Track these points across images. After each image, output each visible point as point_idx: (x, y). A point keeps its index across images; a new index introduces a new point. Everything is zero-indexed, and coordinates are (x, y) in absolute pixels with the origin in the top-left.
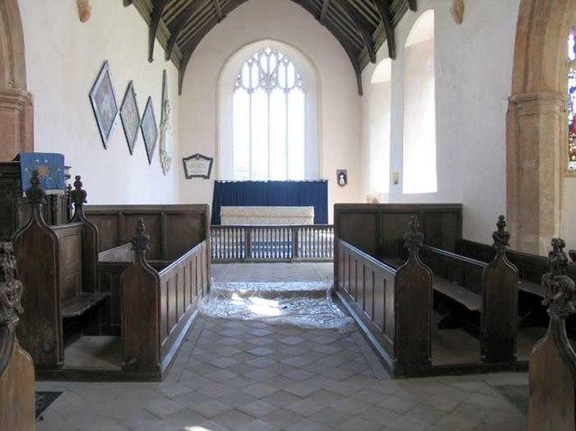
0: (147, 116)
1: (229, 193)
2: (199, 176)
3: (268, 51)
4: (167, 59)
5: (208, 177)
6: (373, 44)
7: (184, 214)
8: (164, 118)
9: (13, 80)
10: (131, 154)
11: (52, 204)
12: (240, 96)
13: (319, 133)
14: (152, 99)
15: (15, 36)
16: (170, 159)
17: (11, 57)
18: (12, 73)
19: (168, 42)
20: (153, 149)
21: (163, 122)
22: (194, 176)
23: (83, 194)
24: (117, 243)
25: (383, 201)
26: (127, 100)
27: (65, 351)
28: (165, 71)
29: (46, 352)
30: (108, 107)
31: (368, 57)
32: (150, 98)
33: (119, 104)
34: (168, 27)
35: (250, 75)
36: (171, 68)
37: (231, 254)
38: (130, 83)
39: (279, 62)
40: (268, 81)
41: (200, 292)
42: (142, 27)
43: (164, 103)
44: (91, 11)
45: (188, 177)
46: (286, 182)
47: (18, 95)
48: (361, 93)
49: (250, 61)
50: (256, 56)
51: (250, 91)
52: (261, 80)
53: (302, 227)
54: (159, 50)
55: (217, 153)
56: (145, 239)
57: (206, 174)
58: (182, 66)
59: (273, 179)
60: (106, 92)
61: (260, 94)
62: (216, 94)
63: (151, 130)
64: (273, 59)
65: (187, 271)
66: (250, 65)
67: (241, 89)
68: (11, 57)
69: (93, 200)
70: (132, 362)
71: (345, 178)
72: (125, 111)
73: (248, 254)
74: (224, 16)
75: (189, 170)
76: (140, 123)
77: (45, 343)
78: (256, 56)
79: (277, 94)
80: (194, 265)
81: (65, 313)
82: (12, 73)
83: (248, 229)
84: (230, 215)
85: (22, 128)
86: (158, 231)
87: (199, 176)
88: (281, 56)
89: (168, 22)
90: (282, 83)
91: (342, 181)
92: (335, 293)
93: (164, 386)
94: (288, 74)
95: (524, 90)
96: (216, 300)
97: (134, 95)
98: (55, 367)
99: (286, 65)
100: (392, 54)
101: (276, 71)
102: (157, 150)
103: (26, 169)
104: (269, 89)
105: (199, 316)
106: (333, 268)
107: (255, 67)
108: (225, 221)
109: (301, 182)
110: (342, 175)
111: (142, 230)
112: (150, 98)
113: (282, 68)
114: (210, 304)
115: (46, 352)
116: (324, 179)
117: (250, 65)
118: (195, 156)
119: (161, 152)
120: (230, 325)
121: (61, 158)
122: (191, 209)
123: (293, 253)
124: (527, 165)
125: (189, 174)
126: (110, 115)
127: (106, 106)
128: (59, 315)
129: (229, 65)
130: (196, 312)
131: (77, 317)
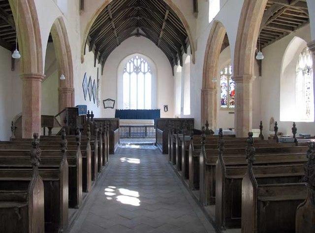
1: (123, 114)
2: (109, 107)
3: (137, 57)
5: (113, 108)
6: (186, 44)
12: (126, 75)
13: (157, 87)
21: (98, 87)
23: (93, 115)
25: (180, 117)
30: (91, 89)
31: (183, 51)
35: (130, 67)
36: (99, 66)
39: (141, 62)
40: (137, 69)
43: (98, 80)
46: (144, 110)
48: (173, 75)
49: (130, 61)
50: (132, 59)
51: (130, 73)
52: (134, 69)
53: (148, 126)
55: (116, 98)
58: (103, 64)
59: (139, 109)
61: (134, 75)
62: (117, 77)
64: (139, 61)
66: (130, 63)
67: (126, 73)
69: (95, 117)
71: (167, 108)
73: (130, 135)
74: (120, 44)
78: (132, 59)
79: (141, 74)
83: (130, 127)
84: (123, 122)
85: (72, 97)
87: (109, 107)
88: (142, 59)
90: (143, 70)
91: (166, 109)
92: (155, 145)
94: (145, 67)
95: (205, 88)
99: (144, 63)
100: (181, 65)
101: (140, 65)
104: (137, 73)
106: (124, 108)
107: (132, 64)
108: (120, 125)
109: (150, 110)
110: (166, 107)
113: (143, 64)
116: (159, 108)
117: (130, 63)
118: (108, 100)
121: (86, 106)
123: (145, 135)
124: (206, 108)
125: (106, 106)
129: (121, 64)
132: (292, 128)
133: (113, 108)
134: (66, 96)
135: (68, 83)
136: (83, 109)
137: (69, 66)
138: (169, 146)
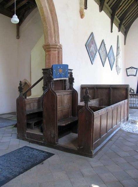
0: (110, 52)
4: (119, 31)
7: (118, 88)
8: (118, 53)
9: (55, 41)
10: (103, 67)
11: (65, 83)
14: (112, 46)
15: (56, 25)
16: (120, 69)
17: (55, 33)
18: (55, 38)
19: (112, 15)
20: (113, 65)
21: (117, 55)
22: (130, 75)
24: (93, 98)
26: (102, 47)
27: (59, 140)
28: (118, 36)
29: (52, 138)
32: (111, 46)
33: (98, 48)
34: (119, 19)
36: (121, 35)
37: (134, 105)
38: (92, 33)
41: (122, 120)
42: (109, 20)
44: (85, 14)
45: (128, 76)
47: (56, 46)
54: (115, 28)
56: (88, 97)
57: (135, 74)
58: (125, 34)
60: (92, 44)
63: (112, 58)
65: (116, 111)
68: (55, 33)
70: (81, 147)
72: (100, 51)
75: (128, 73)
76: (107, 55)
77: (52, 135)
80: (119, 110)
81: (59, 124)
82: (55, 38)
85: (59, 57)
86: (109, 94)
89: (111, 6)
93: (93, 161)
96: (130, 124)
97: (104, 45)
98: (55, 144)
102: (115, 65)
103: (55, 70)
105: (120, 130)
111: (87, 93)
112: (111, 46)
114: (127, 125)
115: (52, 138)
118: (130, 68)
119: (116, 66)
120: (133, 136)
122: (122, 86)
125: (128, 74)
126: (94, 52)
127: (92, 49)
128: (56, 125)
130: (119, 128)
131: (63, 126)
132: (19, 88)
133: (135, 76)
134: (50, 55)
135: (52, 39)
136: (61, 71)
137: (52, 14)
138: (121, 4)
